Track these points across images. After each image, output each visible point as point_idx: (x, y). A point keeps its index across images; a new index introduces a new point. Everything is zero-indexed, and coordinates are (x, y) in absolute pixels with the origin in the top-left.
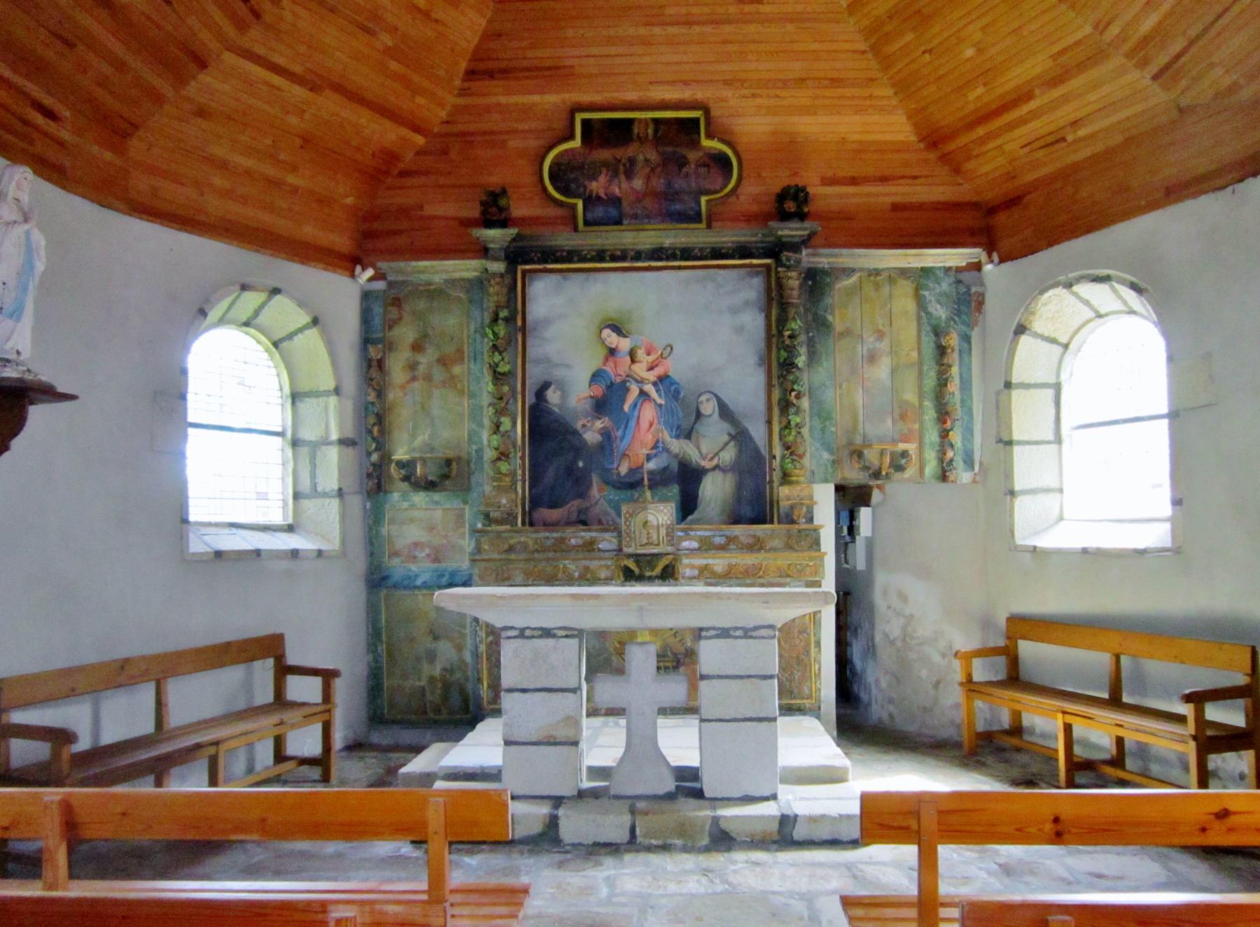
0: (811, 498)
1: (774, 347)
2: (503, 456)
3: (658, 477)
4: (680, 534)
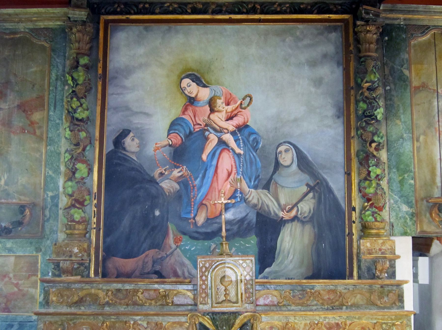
0: (393, 251)
1: (352, 98)
2: (78, 203)
3: (235, 228)
4: (258, 288)
